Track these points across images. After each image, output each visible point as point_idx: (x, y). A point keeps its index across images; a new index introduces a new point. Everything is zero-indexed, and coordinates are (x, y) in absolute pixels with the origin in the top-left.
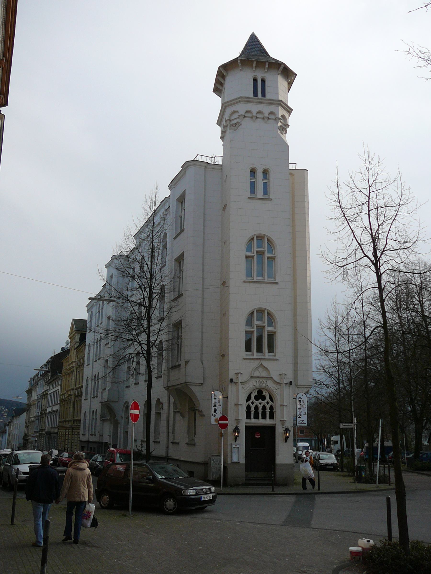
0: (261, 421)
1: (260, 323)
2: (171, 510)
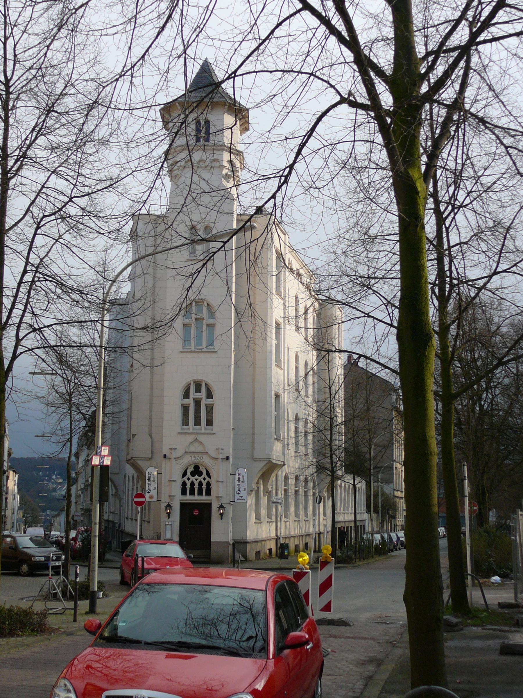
0: (196, 498)
1: (198, 395)
2: (25, 573)
